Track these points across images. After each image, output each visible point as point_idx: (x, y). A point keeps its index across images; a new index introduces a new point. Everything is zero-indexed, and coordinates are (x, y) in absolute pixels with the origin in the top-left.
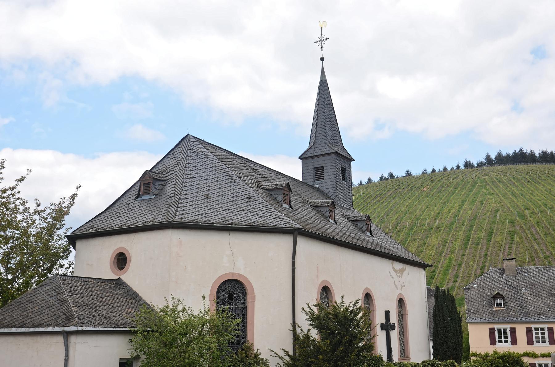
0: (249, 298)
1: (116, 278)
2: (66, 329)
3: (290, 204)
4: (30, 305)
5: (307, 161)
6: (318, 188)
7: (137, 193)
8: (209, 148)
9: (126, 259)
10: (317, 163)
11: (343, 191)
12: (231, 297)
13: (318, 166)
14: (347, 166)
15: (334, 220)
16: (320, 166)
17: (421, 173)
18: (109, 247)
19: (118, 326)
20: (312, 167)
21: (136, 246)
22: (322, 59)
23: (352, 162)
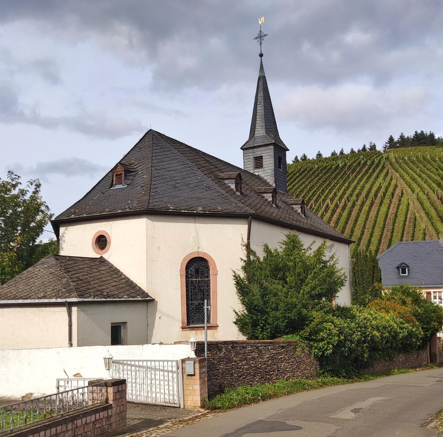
0: (211, 272)
1: (98, 256)
2: (69, 300)
3: (241, 192)
4: (32, 280)
5: (247, 151)
6: (258, 175)
7: (110, 183)
8: (169, 142)
9: (106, 241)
10: (257, 153)
11: (280, 178)
12: (197, 271)
13: (258, 156)
14: (283, 155)
15: (276, 205)
16: (259, 155)
17: (330, 156)
18: (91, 230)
19: (109, 297)
20: (252, 157)
21: (114, 229)
22: (261, 55)
23: (287, 152)
